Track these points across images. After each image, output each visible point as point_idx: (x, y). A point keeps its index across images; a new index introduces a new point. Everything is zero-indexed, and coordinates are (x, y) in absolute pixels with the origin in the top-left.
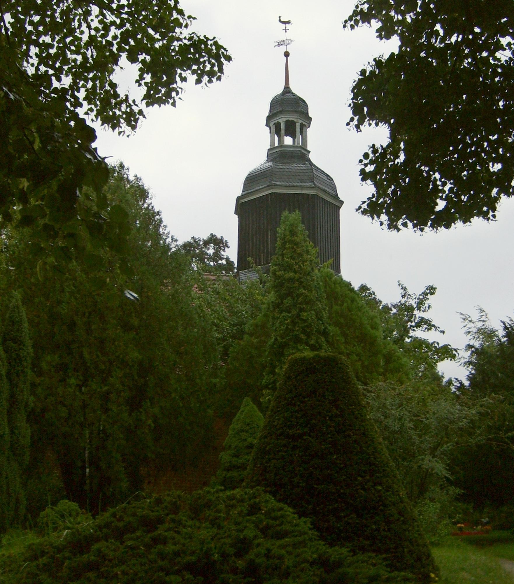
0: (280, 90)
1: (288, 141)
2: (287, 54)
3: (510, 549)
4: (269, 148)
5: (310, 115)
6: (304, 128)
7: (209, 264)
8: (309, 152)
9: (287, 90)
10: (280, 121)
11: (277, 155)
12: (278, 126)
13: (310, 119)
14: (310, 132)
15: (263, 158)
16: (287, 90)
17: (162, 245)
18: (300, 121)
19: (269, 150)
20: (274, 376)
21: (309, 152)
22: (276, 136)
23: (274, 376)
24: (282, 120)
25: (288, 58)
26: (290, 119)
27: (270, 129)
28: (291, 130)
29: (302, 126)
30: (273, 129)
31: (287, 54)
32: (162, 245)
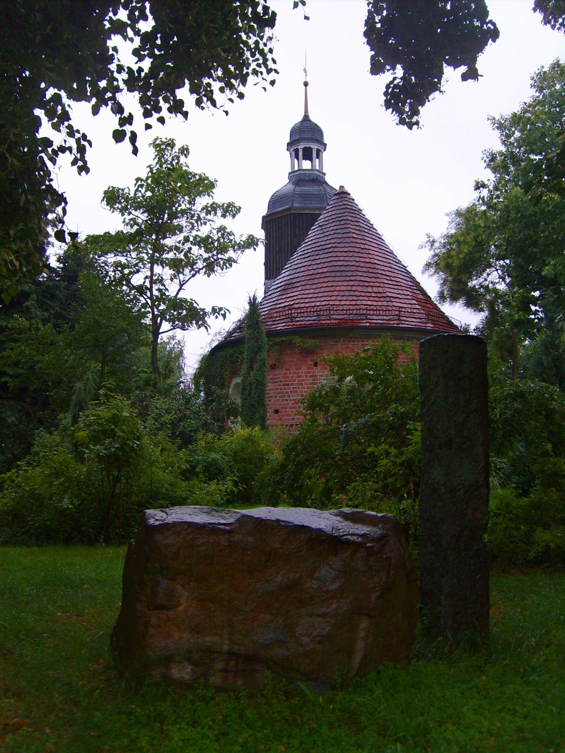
0: (299, 118)
1: (306, 165)
2: (306, 84)
3: (562, 527)
4: (290, 171)
5: (325, 141)
6: (320, 153)
7: (157, 39)
8: (325, 174)
9: (306, 118)
10: (299, 147)
11: (298, 178)
12: (297, 151)
13: (325, 145)
14: (325, 155)
15: (285, 180)
16: (306, 118)
17: (399, 67)
18: (316, 147)
19: (290, 173)
20: (123, 80)
21: (325, 174)
22: (296, 160)
23: (123, 80)
24: (301, 146)
25: (307, 87)
26: (308, 146)
27: (291, 154)
28: (308, 155)
29: (318, 152)
30: (293, 153)
31: (306, 84)
32: (399, 67)
